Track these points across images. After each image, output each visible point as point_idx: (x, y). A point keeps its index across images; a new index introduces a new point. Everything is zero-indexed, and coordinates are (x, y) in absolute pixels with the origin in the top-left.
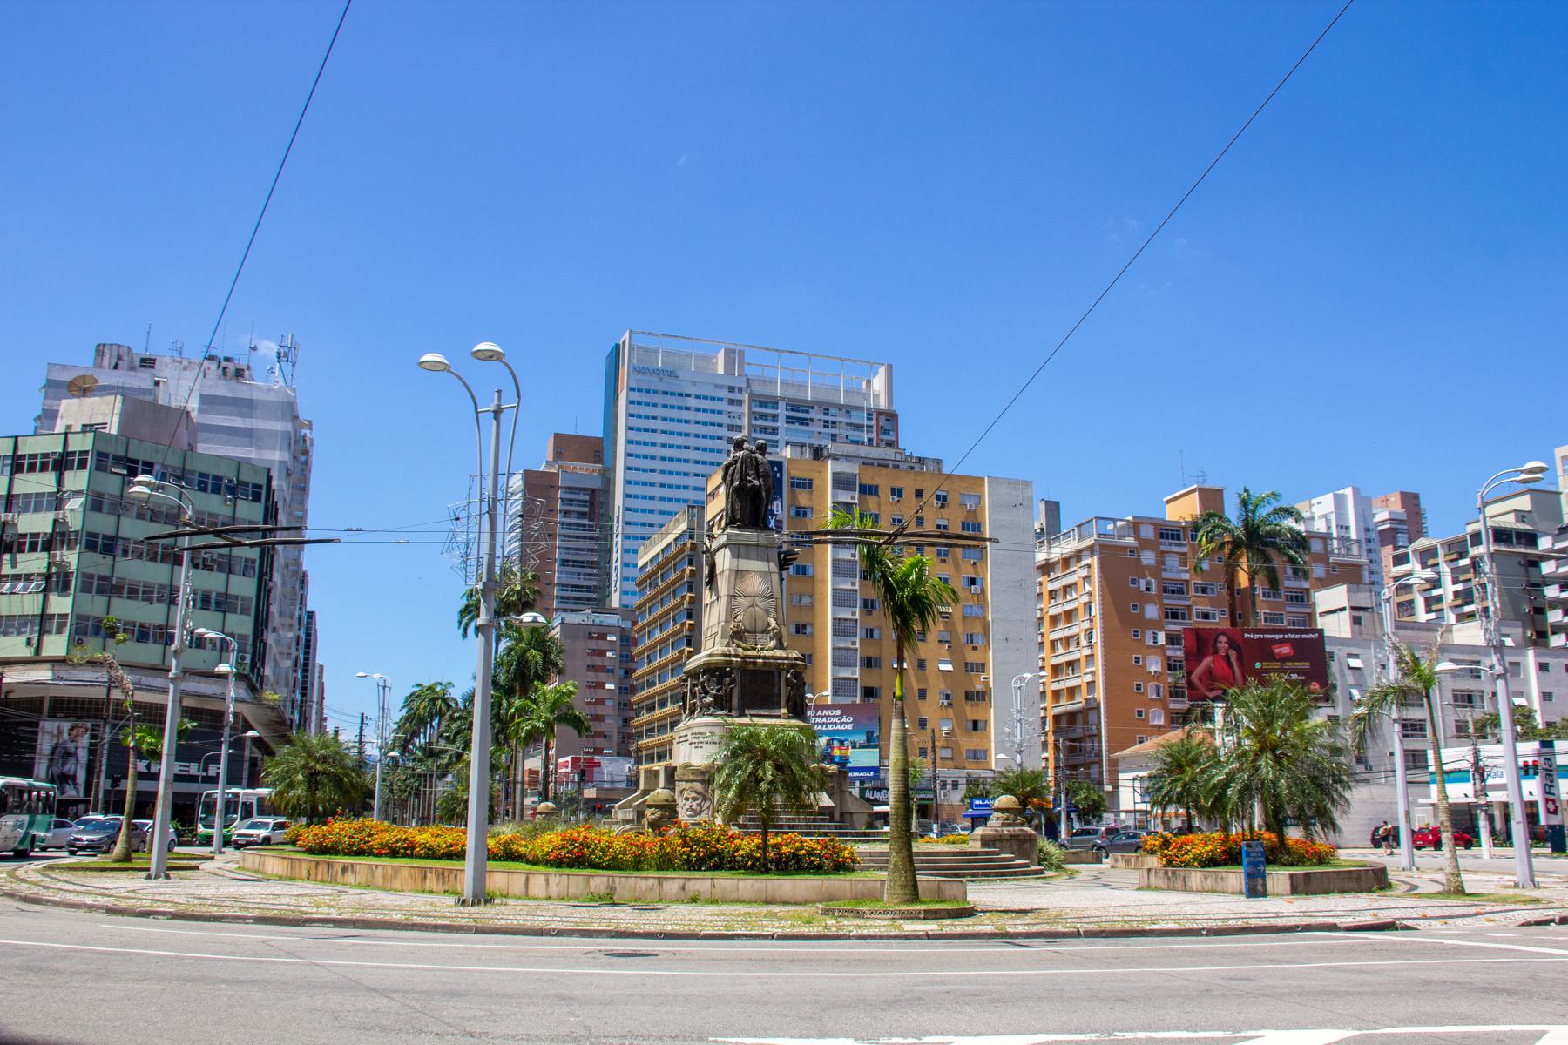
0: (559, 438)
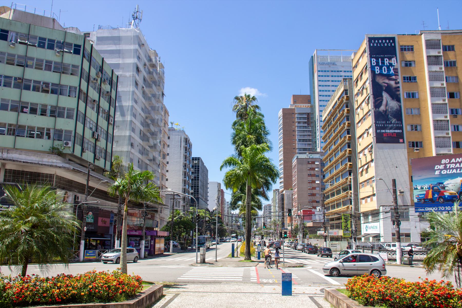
0: (294, 96)
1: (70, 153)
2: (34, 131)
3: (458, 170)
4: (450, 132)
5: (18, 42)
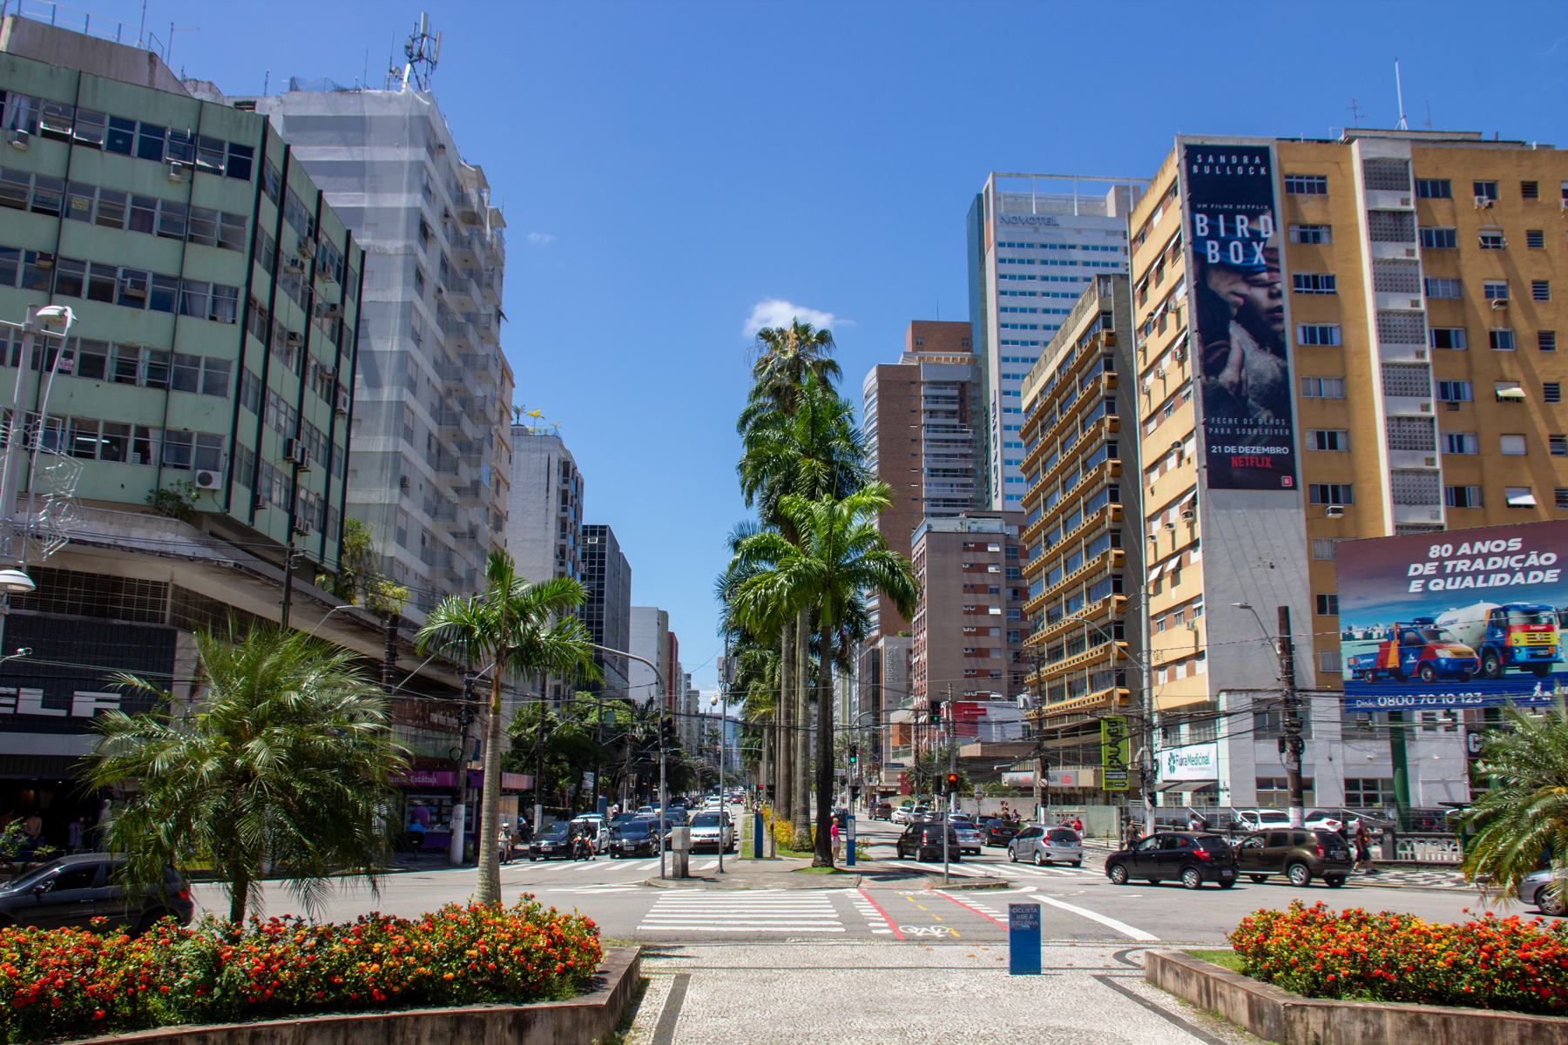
0: (918, 326)
1: (217, 510)
2: (95, 436)
3: (1481, 578)
4: (1437, 455)
5: (39, 133)
